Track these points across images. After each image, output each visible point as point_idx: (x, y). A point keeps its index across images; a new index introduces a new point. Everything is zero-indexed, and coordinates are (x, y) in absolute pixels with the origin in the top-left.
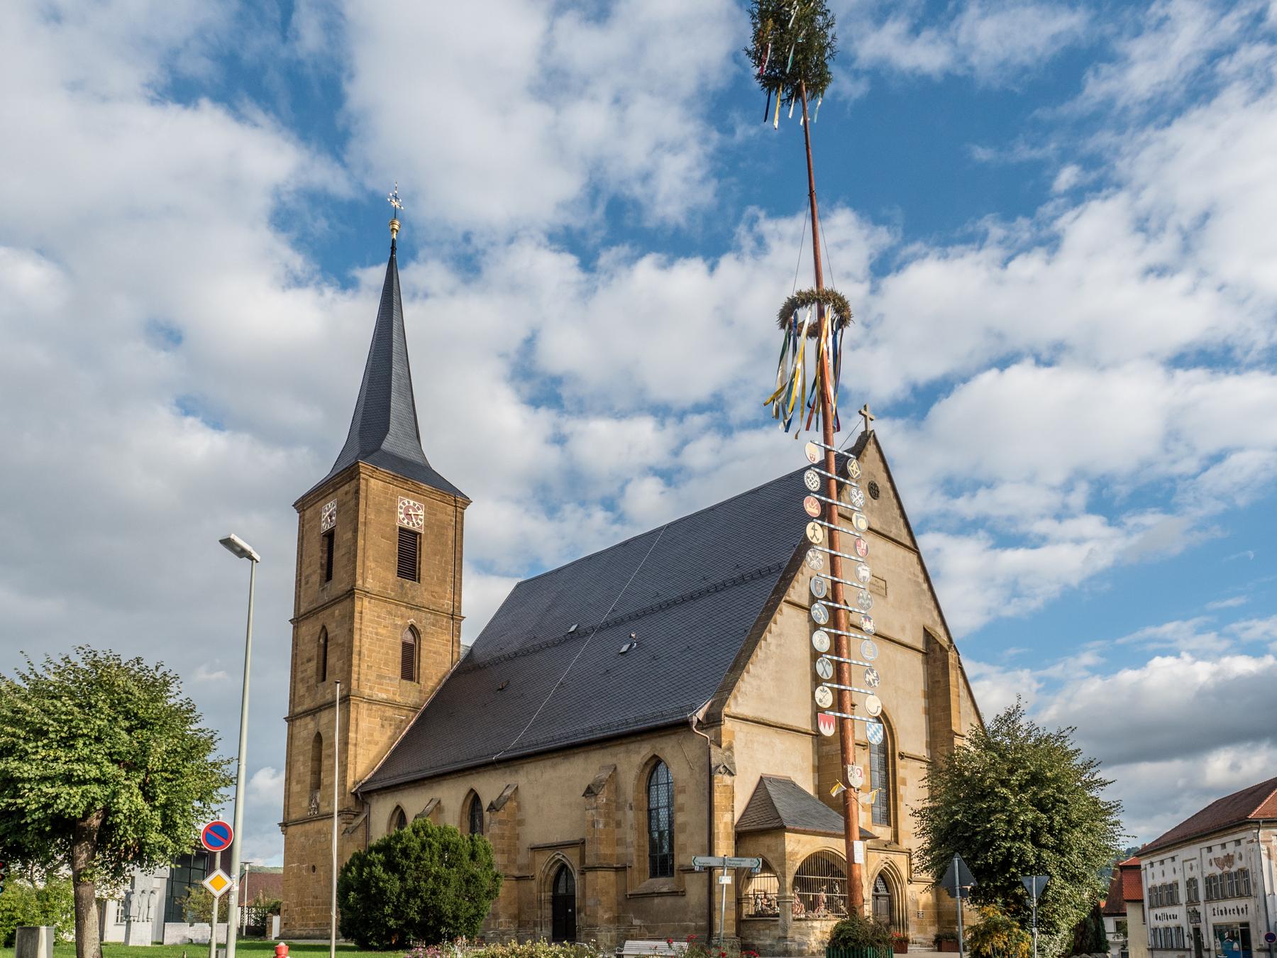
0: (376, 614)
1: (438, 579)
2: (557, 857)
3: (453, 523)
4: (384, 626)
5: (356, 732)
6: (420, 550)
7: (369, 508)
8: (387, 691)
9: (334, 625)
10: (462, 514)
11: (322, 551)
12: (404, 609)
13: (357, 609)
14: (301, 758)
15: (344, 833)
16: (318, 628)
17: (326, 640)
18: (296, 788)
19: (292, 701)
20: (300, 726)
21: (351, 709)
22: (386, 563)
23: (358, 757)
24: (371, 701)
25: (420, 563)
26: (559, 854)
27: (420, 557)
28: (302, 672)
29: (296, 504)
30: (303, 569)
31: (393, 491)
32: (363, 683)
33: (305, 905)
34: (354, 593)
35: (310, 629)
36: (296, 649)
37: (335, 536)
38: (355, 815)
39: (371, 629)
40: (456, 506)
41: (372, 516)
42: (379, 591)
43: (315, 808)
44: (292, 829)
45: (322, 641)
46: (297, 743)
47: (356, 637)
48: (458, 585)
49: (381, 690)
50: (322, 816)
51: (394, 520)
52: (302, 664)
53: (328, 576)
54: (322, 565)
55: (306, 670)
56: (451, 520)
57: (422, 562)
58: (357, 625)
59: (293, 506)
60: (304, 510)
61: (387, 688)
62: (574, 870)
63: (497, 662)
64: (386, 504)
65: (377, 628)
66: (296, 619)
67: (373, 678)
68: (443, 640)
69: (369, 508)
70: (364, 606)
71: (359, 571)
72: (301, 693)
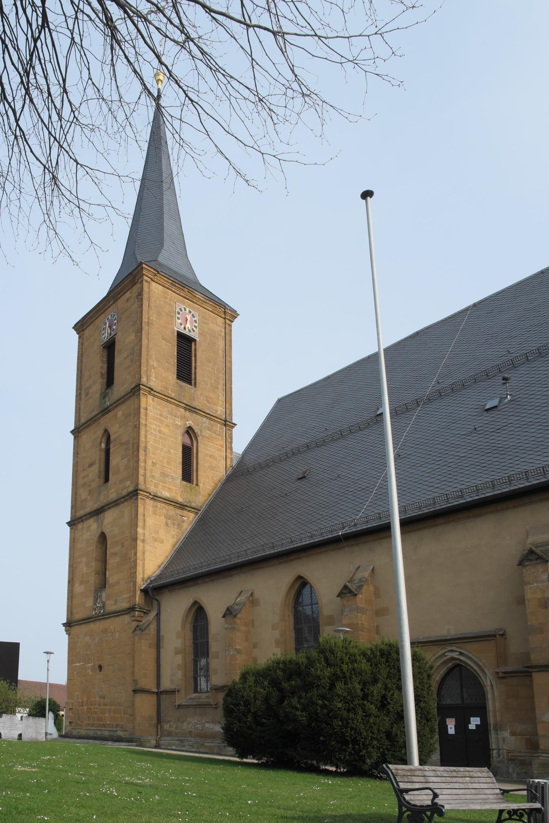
0: (159, 412)
1: (212, 385)
2: (450, 655)
3: (223, 334)
4: (166, 425)
5: (144, 528)
6: (195, 356)
7: (151, 309)
8: (170, 490)
9: (117, 426)
10: (230, 326)
11: (102, 361)
12: (183, 410)
13: (143, 405)
14: (84, 560)
15: (134, 631)
16: (100, 432)
17: (108, 441)
18: (79, 588)
19: (74, 507)
20: (83, 528)
21: (139, 504)
22: (167, 364)
23: (146, 554)
24: (155, 497)
25: (195, 368)
26: (452, 651)
27: (195, 362)
28: (84, 478)
29: (76, 325)
30: (82, 383)
31: (172, 297)
32: (149, 479)
33: (91, 704)
34: (140, 389)
35: (89, 437)
36: (77, 457)
37: (117, 343)
38: (144, 613)
39: (154, 426)
40: (225, 318)
41: (154, 318)
42: (161, 390)
43: (101, 607)
44: (76, 629)
45: (103, 446)
46: (79, 546)
47: (142, 433)
48: (229, 393)
49: (164, 488)
50: (109, 614)
51: (172, 324)
52: (83, 470)
53: (110, 381)
54: (102, 374)
55: (87, 476)
56: (221, 331)
57: (197, 367)
58: (142, 421)
59: (73, 328)
60: (83, 330)
61: (170, 487)
62: (483, 671)
63: (261, 467)
64: (165, 308)
65: (160, 426)
66: (78, 428)
67: (157, 475)
68: (217, 445)
69: (151, 309)
70: (148, 403)
71: (144, 368)
72: (83, 497)
